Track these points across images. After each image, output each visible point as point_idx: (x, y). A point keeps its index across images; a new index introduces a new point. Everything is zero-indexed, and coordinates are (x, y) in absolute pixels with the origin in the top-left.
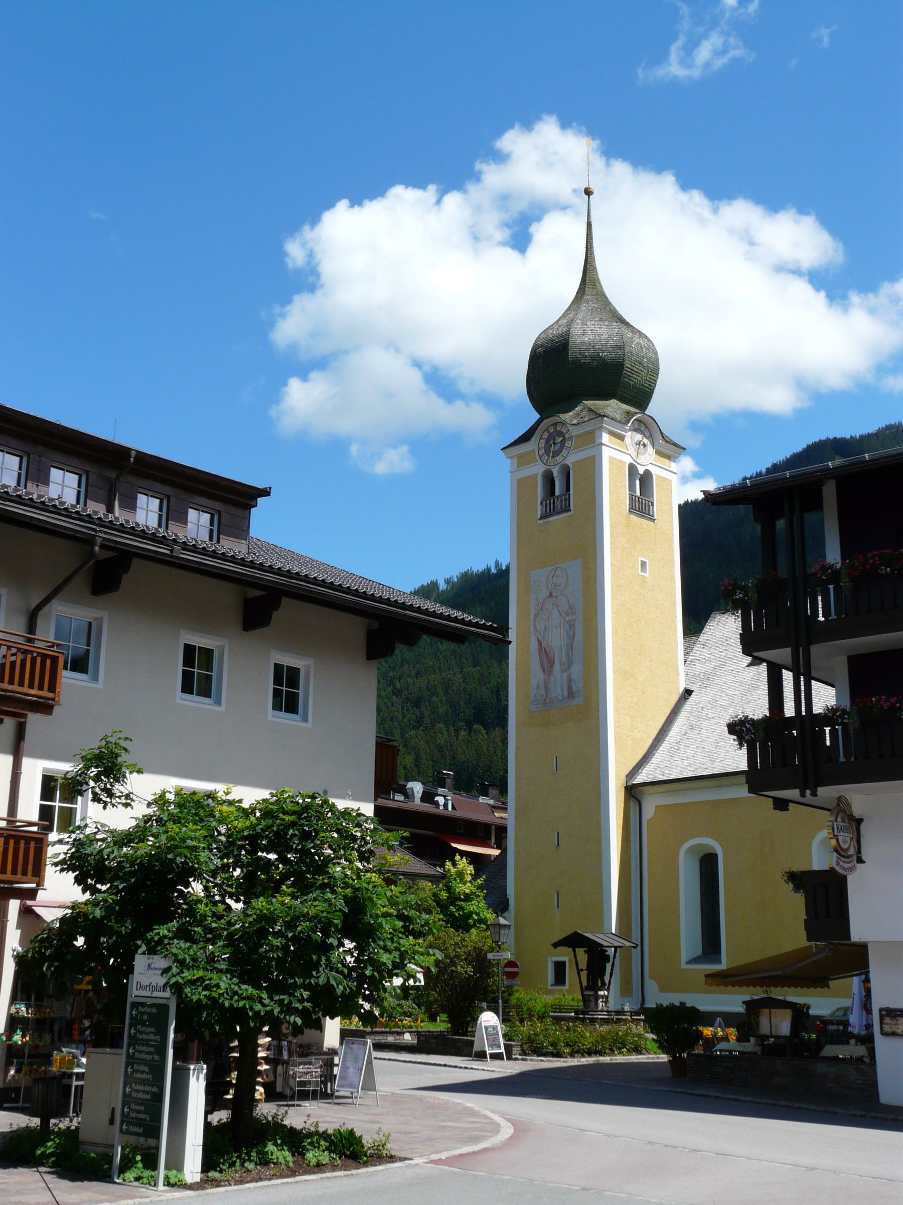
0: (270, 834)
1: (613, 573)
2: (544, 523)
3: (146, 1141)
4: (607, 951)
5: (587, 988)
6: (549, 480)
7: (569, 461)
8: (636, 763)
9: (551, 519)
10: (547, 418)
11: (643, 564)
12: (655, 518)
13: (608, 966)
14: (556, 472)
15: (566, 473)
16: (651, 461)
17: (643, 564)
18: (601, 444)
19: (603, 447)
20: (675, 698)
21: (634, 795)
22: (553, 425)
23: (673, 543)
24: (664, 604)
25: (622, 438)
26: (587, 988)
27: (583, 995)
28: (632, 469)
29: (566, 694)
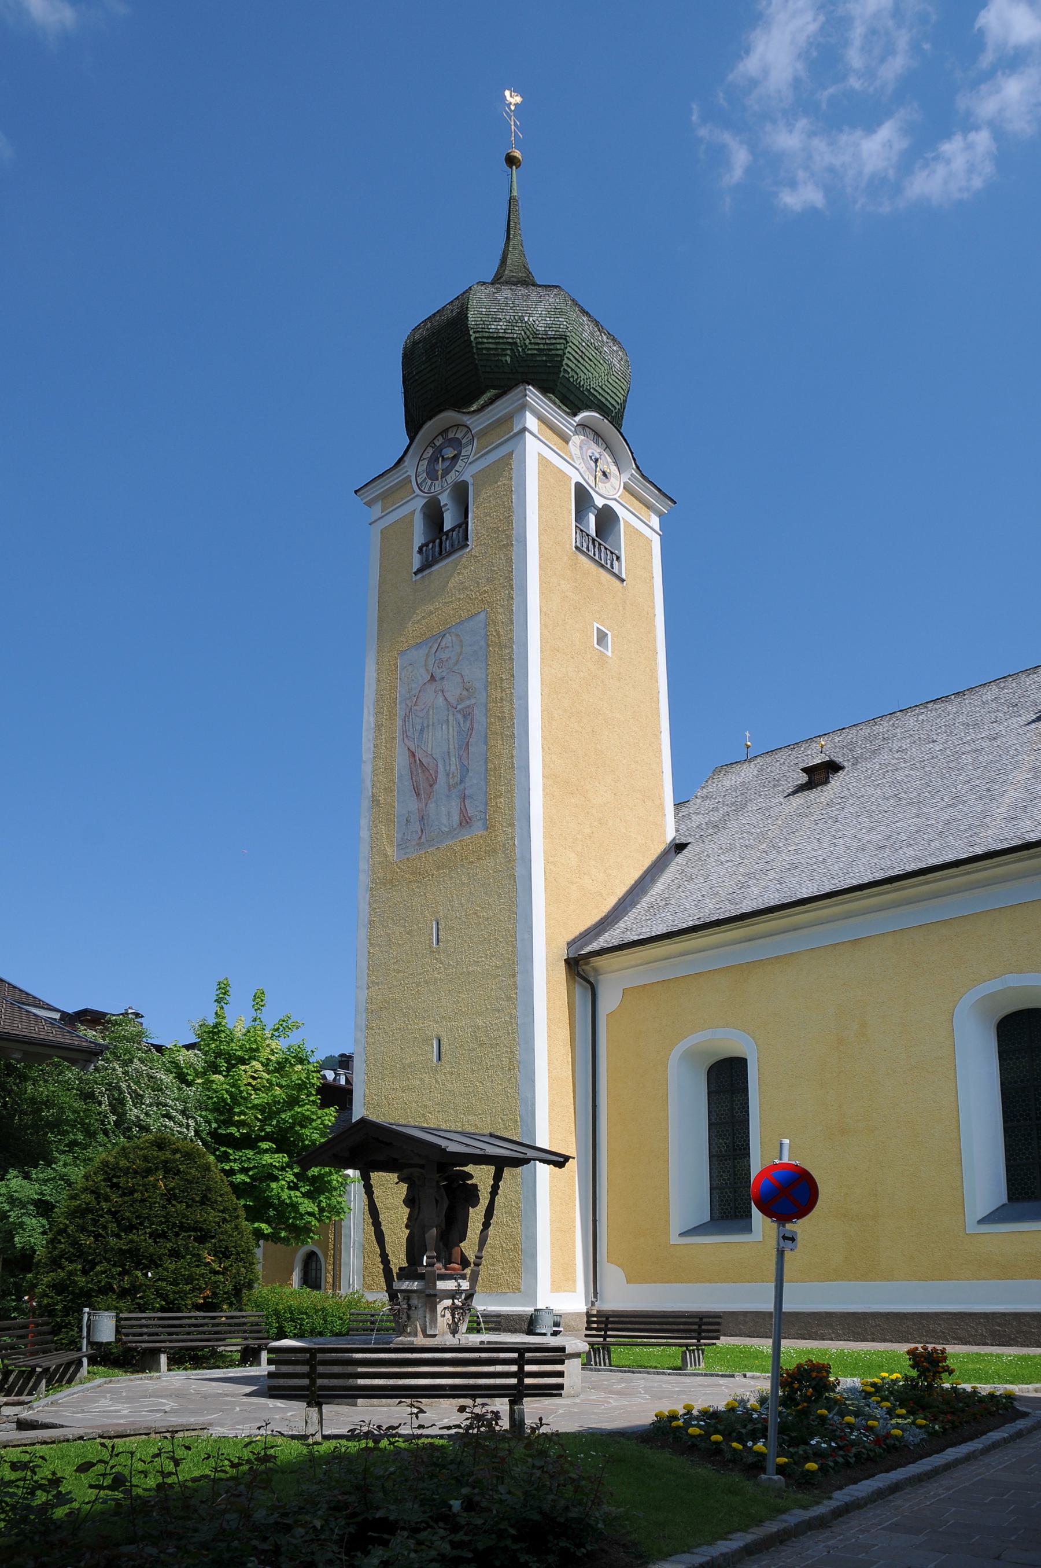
0: (157, 1211)
1: (544, 626)
2: (423, 577)
3: (367, 1444)
4: (471, 1177)
5: (405, 1274)
6: (433, 514)
7: (467, 477)
8: (586, 928)
9: (434, 568)
10: (430, 418)
11: (602, 637)
12: (624, 576)
13: (476, 1216)
14: (444, 499)
15: (461, 493)
16: (616, 496)
17: (602, 637)
18: (525, 429)
19: (527, 433)
20: (658, 849)
21: (582, 973)
22: (441, 434)
23: (655, 626)
24: (639, 706)
25: (566, 440)
26: (405, 1274)
27: (393, 1295)
28: (582, 498)
29: (456, 818)
